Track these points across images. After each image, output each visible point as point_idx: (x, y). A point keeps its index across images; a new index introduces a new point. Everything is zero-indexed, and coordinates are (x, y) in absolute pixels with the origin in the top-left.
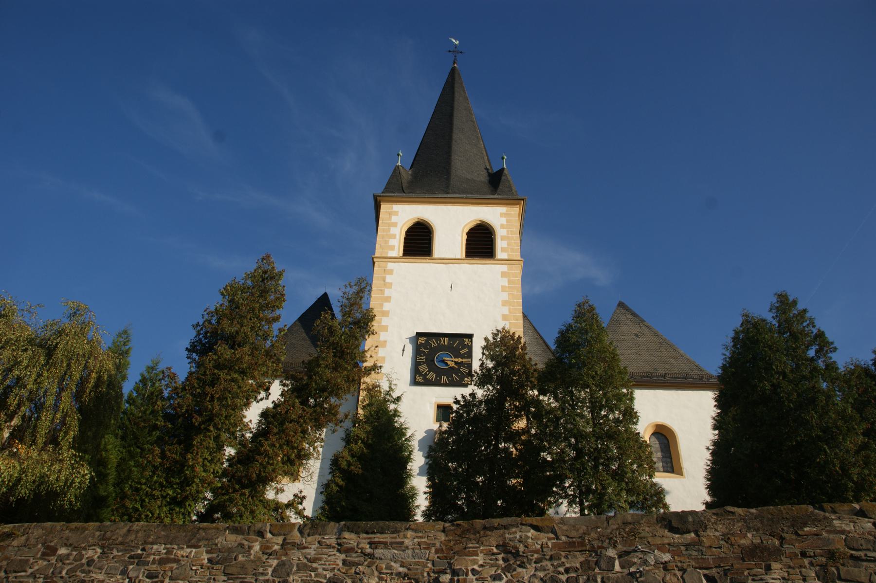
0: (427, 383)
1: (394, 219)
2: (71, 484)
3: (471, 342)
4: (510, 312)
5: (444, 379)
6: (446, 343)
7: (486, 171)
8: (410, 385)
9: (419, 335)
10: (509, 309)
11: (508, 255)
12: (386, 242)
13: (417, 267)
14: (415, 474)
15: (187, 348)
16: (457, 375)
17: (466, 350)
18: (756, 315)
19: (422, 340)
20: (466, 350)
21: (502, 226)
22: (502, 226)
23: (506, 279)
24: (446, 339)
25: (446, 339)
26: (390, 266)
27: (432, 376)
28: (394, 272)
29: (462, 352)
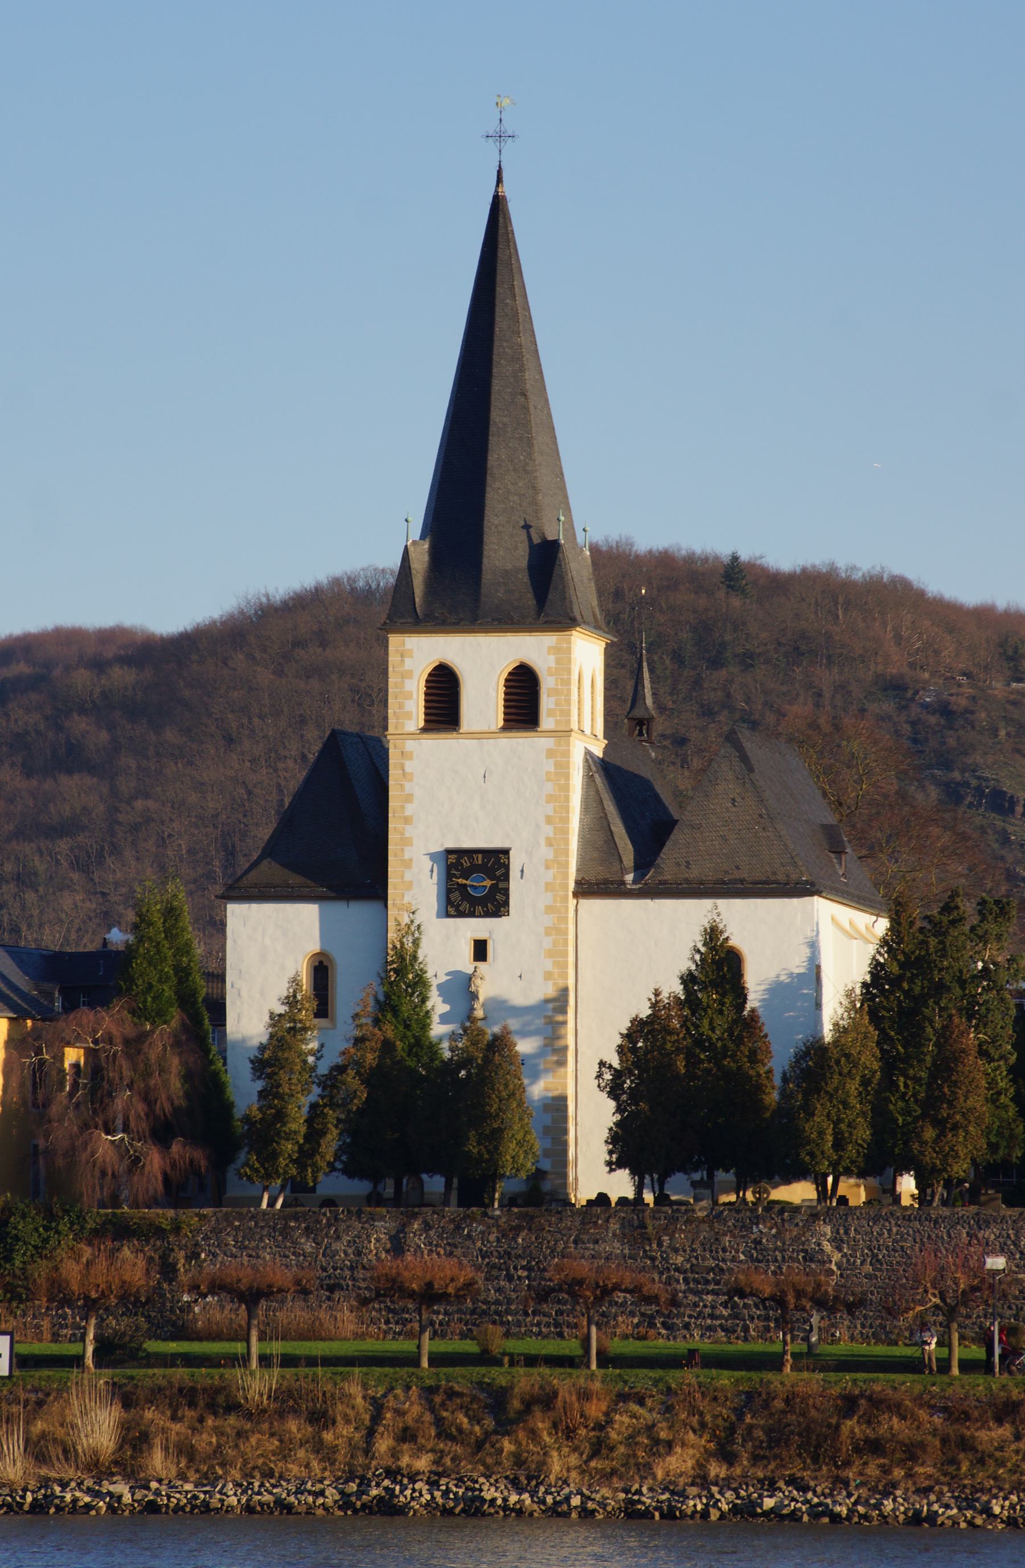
0: (461, 914)
1: (408, 663)
2: (415, 1255)
3: (508, 858)
4: (555, 812)
5: (479, 909)
6: (480, 862)
7: (806, 952)
8: (439, 916)
9: (449, 852)
10: (555, 807)
11: (557, 721)
12: (401, 706)
13: (441, 744)
14: (697, 1191)
15: (609, 1164)
16: (493, 904)
17: (503, 871)
18: (655, 548)
19: (452, 858)
20: (503, 871)
21: (550, 673)
22: (550, 673)
23: (551, 761)
24: (480, 856)
25: (480, 856)
26: (410, 745)
27: (465, 906)
28: (415, 755)
29: (498, 873)
